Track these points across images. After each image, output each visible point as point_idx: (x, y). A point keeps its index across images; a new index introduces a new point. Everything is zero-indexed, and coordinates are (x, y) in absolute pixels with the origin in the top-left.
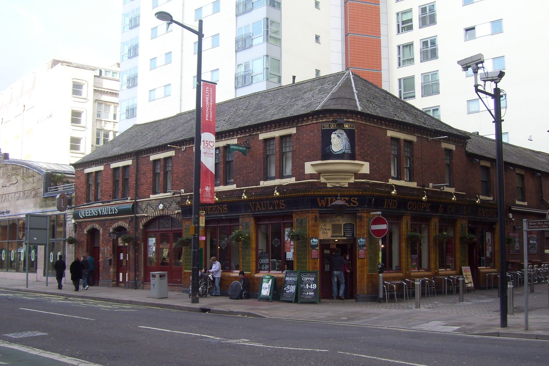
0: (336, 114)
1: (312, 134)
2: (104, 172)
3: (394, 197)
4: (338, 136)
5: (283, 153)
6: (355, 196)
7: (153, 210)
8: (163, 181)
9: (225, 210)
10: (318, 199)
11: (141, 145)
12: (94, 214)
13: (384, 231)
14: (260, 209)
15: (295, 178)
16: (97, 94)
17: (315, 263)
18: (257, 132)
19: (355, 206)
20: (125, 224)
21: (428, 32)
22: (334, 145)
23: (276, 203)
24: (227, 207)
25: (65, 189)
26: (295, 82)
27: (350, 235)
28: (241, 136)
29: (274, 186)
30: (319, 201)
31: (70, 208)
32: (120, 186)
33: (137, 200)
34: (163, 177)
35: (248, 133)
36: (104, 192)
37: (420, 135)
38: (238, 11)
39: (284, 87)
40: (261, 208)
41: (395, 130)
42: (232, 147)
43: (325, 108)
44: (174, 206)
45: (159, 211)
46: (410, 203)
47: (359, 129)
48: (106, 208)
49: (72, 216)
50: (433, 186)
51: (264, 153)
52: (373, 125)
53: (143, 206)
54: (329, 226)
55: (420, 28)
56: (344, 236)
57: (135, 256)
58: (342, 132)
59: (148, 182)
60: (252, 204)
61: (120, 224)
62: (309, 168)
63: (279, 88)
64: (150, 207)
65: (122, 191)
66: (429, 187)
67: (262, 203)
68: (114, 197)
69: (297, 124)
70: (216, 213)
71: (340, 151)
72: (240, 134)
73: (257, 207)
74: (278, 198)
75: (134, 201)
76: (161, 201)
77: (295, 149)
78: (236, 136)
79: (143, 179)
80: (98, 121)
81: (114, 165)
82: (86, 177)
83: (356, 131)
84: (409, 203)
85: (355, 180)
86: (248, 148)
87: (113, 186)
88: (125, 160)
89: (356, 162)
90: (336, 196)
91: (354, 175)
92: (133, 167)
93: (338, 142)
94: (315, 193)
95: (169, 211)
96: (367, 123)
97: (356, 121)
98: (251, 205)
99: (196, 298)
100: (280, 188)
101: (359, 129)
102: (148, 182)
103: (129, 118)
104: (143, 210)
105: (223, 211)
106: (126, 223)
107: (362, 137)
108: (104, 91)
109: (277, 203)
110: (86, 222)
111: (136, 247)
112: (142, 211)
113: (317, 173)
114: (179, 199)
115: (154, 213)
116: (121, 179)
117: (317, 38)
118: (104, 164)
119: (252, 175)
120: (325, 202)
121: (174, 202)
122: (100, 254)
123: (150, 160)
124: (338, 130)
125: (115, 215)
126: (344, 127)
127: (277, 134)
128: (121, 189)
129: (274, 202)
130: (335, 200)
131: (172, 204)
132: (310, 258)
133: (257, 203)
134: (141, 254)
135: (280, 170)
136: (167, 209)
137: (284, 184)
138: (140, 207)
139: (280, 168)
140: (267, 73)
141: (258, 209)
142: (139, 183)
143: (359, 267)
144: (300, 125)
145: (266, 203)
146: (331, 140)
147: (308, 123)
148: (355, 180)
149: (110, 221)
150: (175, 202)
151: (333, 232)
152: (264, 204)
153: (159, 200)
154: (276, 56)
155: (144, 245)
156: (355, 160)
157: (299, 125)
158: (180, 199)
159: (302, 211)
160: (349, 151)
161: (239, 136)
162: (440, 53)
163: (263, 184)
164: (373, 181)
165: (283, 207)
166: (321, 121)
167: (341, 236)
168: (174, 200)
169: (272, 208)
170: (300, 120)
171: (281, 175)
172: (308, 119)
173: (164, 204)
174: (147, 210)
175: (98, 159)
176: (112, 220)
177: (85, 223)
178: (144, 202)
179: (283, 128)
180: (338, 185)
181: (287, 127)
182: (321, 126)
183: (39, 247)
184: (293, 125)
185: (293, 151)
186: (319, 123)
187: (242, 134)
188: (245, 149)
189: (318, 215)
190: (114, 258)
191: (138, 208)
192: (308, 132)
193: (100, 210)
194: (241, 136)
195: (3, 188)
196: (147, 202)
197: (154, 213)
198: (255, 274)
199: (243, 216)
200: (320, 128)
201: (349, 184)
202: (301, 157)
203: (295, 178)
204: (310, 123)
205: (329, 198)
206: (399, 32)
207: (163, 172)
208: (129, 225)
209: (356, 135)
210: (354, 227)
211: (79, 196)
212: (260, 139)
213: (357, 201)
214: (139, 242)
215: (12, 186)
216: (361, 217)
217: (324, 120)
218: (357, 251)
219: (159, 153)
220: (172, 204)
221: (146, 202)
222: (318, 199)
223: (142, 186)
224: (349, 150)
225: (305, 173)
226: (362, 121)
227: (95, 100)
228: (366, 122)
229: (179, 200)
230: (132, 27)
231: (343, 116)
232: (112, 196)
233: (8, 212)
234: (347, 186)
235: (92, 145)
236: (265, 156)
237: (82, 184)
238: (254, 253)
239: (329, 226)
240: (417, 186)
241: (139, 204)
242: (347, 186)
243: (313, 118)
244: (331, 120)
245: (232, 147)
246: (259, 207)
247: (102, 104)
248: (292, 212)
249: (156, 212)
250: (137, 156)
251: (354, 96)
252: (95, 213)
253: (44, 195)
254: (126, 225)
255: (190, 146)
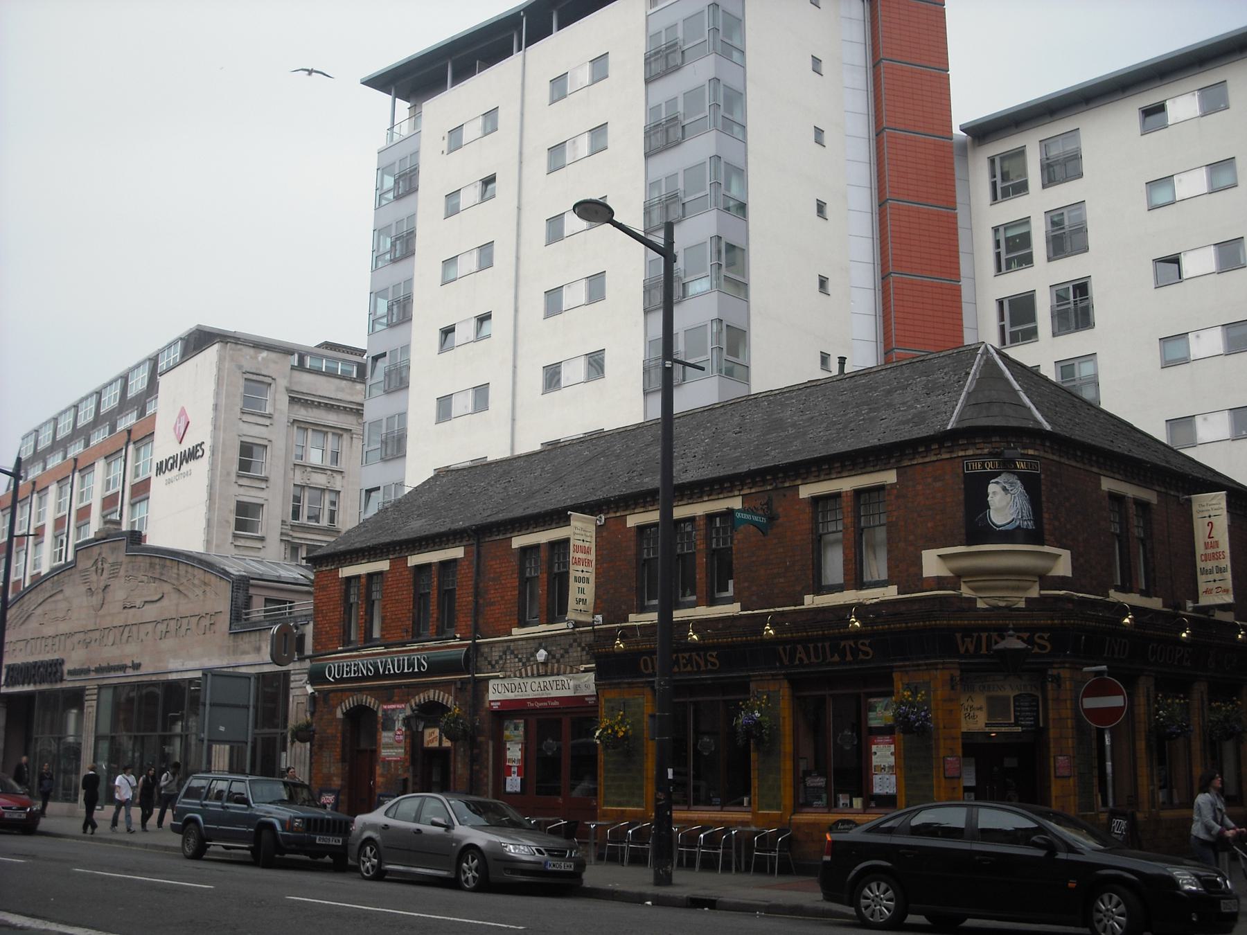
0: (998, 439)
1: (938, 484)
2: (389, 576)
3: (1126, 631)
4: (1004, 489)
5: (862, 530)
6: (1042, 629)
7: (521, 664)
8: (545, 596)
9: (713, 664)
10: (958, 636)
11: (482, 513)
12: (365, 672)
13: (1118, 710)
14: (806, 661)
15: (896, 587)
16: (296, 407)
17: (954, 788)
18: (795, 480)
19: (1044, 652)
20: (444, 695)
21: (1069, 269)
22: (996, 510)
23: (848, 648)
24: (717, 657)
25: (270, 616)
26: (846, 372)
27: (1031, 721)
28: (753, 491)
29: (851, 606)
30: (960, 642)
31: (301, 659)
32: (433, 607)
33: (477, 641)
34: (546, 588)
35: (771, 484)
36: (390, 621)
37: (1163, 490)
38: (650, 222)
39: (823, 382)
40: (809, 658)
41: (1117, 476)
42: (738, 515)
43: (966, 424)
44: (575, 654)
45: (535, 667)
46: (1153, 647)
47: (1048, 473)
48: (396, 659)
49: (306, 677)
50: (1193, 607)
51: (812, 529)
52: (1074, 464)
53: (494, 654)
54: (980, 701)
55: (1049, 260)
56: (1016, 724)
57: (472, 770)
58: (1013, 479)
59: (506, 598)
60: (784, 650)
61: (432, 696)
62: (932, 563)
63: (809, 385)
64: (512, 656)
65: (438, 619)
66: (1185, 610)
67: (811, 646)
68: (416, 636)
69: (898, 462)
70: (689, 672)
71: (1008, 524)
72: (751, 485)
73: (798, 655)
74: (857, 635)
75: (470, 642)
76: (541, 642)
77: (894, 519)
78: (740, 490)
79: (492, 592)
80: (297, 467)
81: (415, 560)
82: (344, 587)
83: (1043, 476)
84: (1150, 647)
85: (1042, 592)
86: (772, 518)
87: (414, 607)
88: (447, 546)
89: (1046, 549)
90: (1006, 629)
91: (1037, 579)
92: (467, 563)
93: (1004, 503)
94: (952, 622)
95: (562, 666)
96: (1063, 460)
97: (1042, 454)
98: (781, 652)
99: (666, 872)
100: (861, 610)
101: (1048, 473)
102: (506, 598)
103: (389, 460)
104: (494, 663)
105: (706, 666)
106: (447, 695)
107: (1055, 491)
108: (313, 401)
109: (850, 646)
110: (342, 690)
111: (476, 751)
112: (490, 667)
113: (951, 575)
114: (589, 639)
115: (523, 670)
116: (436, 592)
117: (823, 282)
118: (391, 557)
119: (782, 580)
120: (974, 642)
121: (575, 644)
122: (377, 768)
123: (513, 547)
124: (1003, 475)
125: (420, 674)
126: (1016, 468)
127: (846, 485)
128: (435, 615)
129: (842, 644)
130: (999, 639)
131: (570, 650)
132: (942, 776)
133: (800, 647)
134: (487, 768)
135: (856, 568)
136: (558, 662)
137: (868, 602)
138: (486, 659)
139: (856, 563)
140: (720, 357)
141: (801, 660)
142: (481, 601)
143: (1056, 797)
144: (906, 463)
145: (823, 647)
146: (989, 499)
147: (927, 460)
148: (1042, 592)
149: (406, 690)
150: (579, 645)
151: (990, 715)
152: (816, 648)
153: (537, 641)
154: (737, 322)
155: (493, 747)
156: (1042, 544)
157: (905, 464)
158: (592, 638)
159: (918, 665)
160: (1030, 525)
161: (746, 491)
162: (1098, 315)
163: (810, 601)
164: (1081, 595)
165: (868, 656)
166: (961, 453)
167: (1010, 725)
168: (575, 641)
169: (836, 658)
170: (907, 452)
171: (856, 580)
172: (928, 450)
173: (549, 649)
174: (505, 663)
175: (378, 545)
176: (408, 686)
177: (339, 694)
178: (497, 645)
179: (864, 471)
180: (1002, 604)
181: (872, 469)
182: (961, 464)
183: (215, 747)
184: (889, 463)
185: (890, 526)
186: (957, 460)
187: (754, 484)
188: (764, 520)
189: (957, 673)
190: (415, 776)
191: (479, 659)
192: (930, 480)
193: (381, 663)
194: (753, 491)
195: (125, 611)
196: (505, 644)
197: (523, 670)
198: (794, 813)
199: (759, 678)
200: (961, 470)
201: (1028, 600)
202: (911, 538)
203: (896, 587)
204: (934, 458)
205: (984, 635)
206: (999, 269)
207: (545, 575)
208: (456, 699)
209: (1043, 488)
210: (1038, 703)
211: (324, 629)
212: (801, 497)
213: (1048, 640)
214: (481, 739)
215: (147, 607)
216: (1057, 680)
217: (970, 452)
218: (1052, 759)
219: (535, 530)
220: (570, 650)
221: (501, 644)
222: (958, 636)
223: (492, 608)
224: (1030, 520)
225: (924, 576)
226: (1053, 454)
227: (292, 420)
228: (1060, 456)
229: (588, 639)
230: (395, 258)
231: (1014, 443)
232: (411, 630)
233: (136, 666)
234: (1022, 605)
235: (282, 521)
236: (814, 537)
237: (332, 603)
238: (788, 765)
239: (980, 701)
240: (1164, 607)
241: (482, 650)
242: (1022, 605)
243: (940, 448)
244: (986, 451)
245: (738, 515)
246: (803, 656)
247: (307, 429)
248: (892, 667)
249: (529, 668)
250: (479, 539)
251: (1019, 397)
252: (368, 669)
253: (233, 627)
254: (448, 699)
255: (618, 514)
